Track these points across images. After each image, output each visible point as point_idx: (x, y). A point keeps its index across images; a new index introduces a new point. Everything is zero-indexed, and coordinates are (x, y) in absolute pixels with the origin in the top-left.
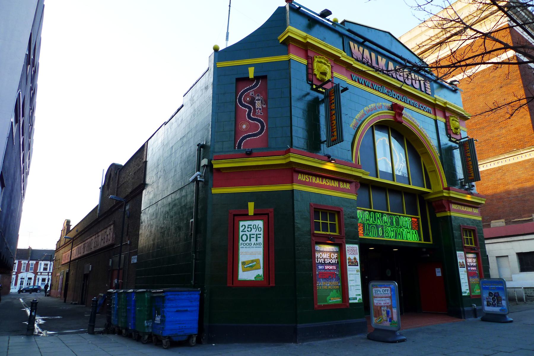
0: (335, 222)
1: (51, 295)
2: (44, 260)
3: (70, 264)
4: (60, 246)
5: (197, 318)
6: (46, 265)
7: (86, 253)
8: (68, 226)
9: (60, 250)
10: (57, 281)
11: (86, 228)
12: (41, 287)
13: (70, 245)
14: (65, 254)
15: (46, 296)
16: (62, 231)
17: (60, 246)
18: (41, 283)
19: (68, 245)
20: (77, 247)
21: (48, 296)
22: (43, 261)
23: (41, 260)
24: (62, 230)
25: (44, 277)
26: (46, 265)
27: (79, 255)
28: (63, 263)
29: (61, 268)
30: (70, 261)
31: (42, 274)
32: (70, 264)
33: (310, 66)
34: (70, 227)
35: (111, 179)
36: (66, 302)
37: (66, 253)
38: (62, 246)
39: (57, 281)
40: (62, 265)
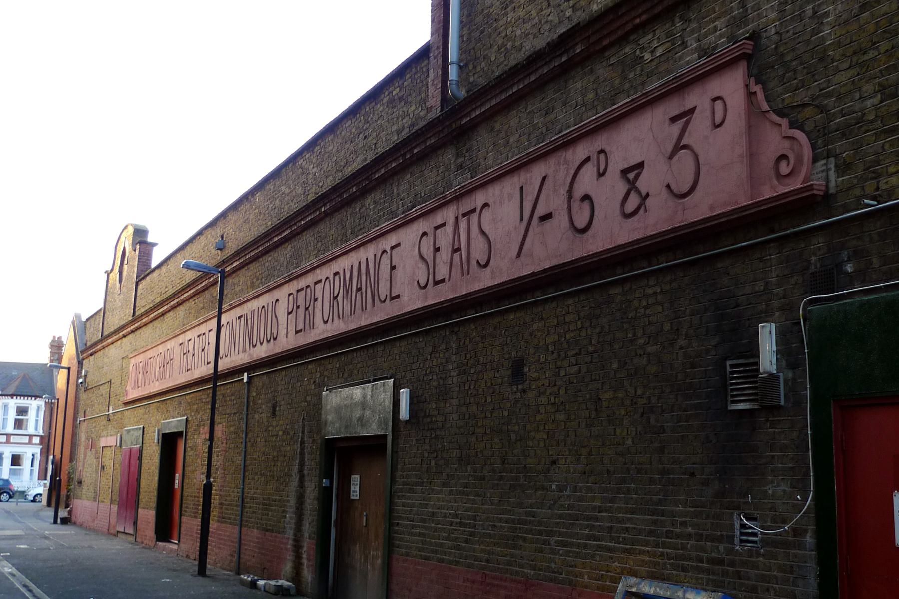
0: (20, 465)
1: (74, 519)
2: (17, 396)
3: (215, 388)
4: (104, 335)
5: (53, 513)
6: (22, 411)
7: (321, 331)
8: (144, 246)
9: (109, 345)
10: (103, 467)
11: (322, 198)
12: (13, 483)
13: (207, 294)
14: (141, 358)
15: (55, 522)
16: (109, 273)
17: (106, 334)
18: (10, 469)
19: (133, 332)
20: (293, 287)
21: (65, 521)
22: (12, 396)
23: (8, 395)
24: (109, 269)
25: (17, 450)
26: (22, 411)
27: (262, 352)
28: (133, 395)
29: (119, 415)
30: (216, 377)
31: (12, 441)
32: (215, 388)
33: (80, 369)
34: (152, 250)
35: (126, 259)
36: (208, 572)
37: (149, 354)
38: (147, 313)
39: (103, 467)
40: (126, 404)
